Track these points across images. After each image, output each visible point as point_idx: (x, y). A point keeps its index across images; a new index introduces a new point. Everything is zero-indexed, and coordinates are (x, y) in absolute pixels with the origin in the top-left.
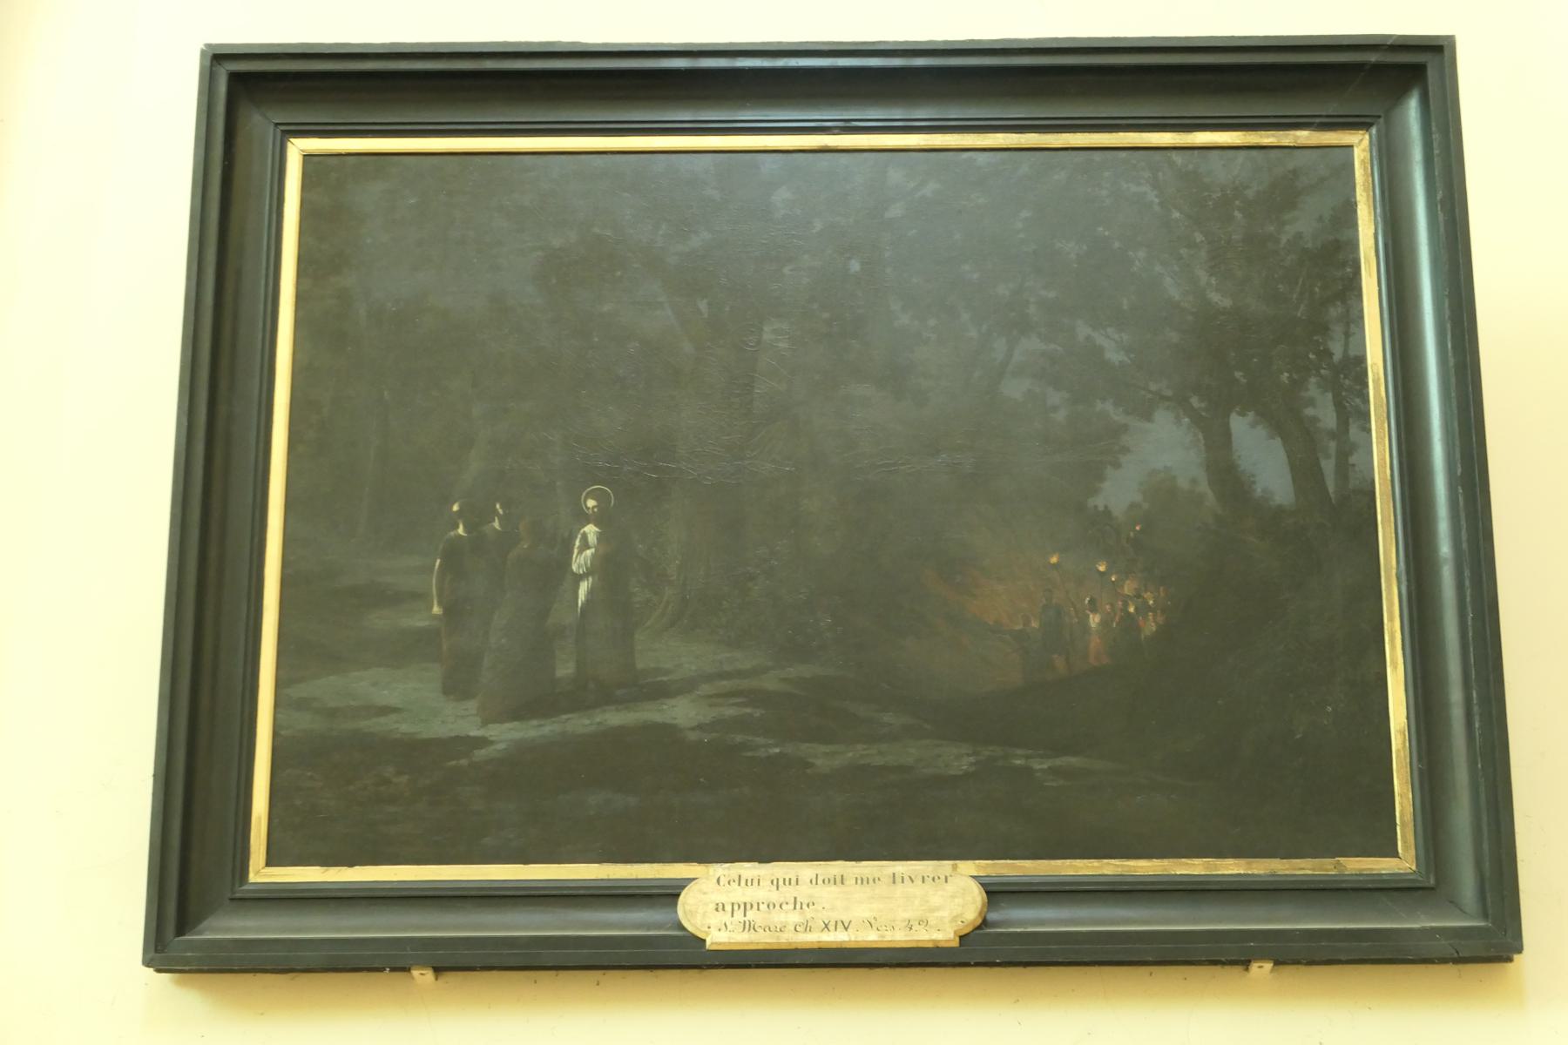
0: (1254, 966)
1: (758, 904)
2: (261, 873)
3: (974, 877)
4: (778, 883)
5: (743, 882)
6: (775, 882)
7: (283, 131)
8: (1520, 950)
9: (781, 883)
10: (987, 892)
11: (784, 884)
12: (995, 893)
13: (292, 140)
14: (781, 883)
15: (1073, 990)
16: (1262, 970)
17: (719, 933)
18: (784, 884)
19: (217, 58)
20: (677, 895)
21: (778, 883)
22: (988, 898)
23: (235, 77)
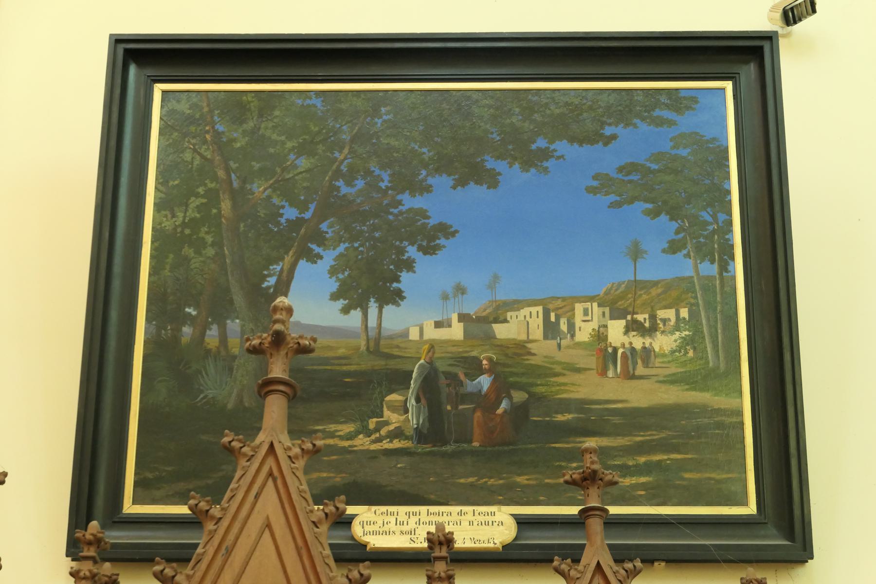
0: (656, 564)
1: (449, 522)
2: (129, 508)
3: (511, 515)
4: (363, 524)
5: (389, 514)
6: (361, 523)
7: (152, 80)
8: (812, 558)
9: (365, 523)
10: (518, 523)
11: (367, 524)
12: (523, 522)
13: (157, 84)
14: (365, 523)
15: (798, 575)
16: (659, 566)
17: (377, 542)
18: (367, 524)
19: (117, 41)
20: (351, 523)
21: (363, 524)
22: (518, 528)
23: (126, 51)
